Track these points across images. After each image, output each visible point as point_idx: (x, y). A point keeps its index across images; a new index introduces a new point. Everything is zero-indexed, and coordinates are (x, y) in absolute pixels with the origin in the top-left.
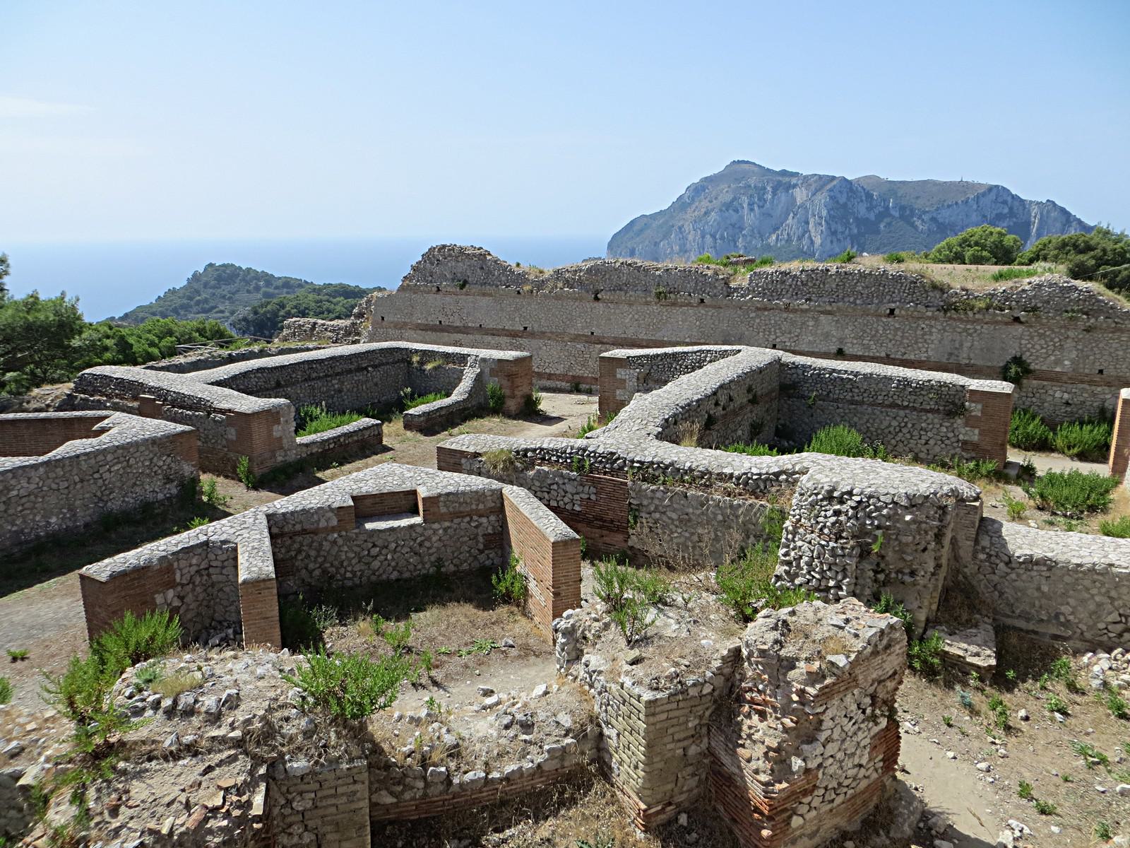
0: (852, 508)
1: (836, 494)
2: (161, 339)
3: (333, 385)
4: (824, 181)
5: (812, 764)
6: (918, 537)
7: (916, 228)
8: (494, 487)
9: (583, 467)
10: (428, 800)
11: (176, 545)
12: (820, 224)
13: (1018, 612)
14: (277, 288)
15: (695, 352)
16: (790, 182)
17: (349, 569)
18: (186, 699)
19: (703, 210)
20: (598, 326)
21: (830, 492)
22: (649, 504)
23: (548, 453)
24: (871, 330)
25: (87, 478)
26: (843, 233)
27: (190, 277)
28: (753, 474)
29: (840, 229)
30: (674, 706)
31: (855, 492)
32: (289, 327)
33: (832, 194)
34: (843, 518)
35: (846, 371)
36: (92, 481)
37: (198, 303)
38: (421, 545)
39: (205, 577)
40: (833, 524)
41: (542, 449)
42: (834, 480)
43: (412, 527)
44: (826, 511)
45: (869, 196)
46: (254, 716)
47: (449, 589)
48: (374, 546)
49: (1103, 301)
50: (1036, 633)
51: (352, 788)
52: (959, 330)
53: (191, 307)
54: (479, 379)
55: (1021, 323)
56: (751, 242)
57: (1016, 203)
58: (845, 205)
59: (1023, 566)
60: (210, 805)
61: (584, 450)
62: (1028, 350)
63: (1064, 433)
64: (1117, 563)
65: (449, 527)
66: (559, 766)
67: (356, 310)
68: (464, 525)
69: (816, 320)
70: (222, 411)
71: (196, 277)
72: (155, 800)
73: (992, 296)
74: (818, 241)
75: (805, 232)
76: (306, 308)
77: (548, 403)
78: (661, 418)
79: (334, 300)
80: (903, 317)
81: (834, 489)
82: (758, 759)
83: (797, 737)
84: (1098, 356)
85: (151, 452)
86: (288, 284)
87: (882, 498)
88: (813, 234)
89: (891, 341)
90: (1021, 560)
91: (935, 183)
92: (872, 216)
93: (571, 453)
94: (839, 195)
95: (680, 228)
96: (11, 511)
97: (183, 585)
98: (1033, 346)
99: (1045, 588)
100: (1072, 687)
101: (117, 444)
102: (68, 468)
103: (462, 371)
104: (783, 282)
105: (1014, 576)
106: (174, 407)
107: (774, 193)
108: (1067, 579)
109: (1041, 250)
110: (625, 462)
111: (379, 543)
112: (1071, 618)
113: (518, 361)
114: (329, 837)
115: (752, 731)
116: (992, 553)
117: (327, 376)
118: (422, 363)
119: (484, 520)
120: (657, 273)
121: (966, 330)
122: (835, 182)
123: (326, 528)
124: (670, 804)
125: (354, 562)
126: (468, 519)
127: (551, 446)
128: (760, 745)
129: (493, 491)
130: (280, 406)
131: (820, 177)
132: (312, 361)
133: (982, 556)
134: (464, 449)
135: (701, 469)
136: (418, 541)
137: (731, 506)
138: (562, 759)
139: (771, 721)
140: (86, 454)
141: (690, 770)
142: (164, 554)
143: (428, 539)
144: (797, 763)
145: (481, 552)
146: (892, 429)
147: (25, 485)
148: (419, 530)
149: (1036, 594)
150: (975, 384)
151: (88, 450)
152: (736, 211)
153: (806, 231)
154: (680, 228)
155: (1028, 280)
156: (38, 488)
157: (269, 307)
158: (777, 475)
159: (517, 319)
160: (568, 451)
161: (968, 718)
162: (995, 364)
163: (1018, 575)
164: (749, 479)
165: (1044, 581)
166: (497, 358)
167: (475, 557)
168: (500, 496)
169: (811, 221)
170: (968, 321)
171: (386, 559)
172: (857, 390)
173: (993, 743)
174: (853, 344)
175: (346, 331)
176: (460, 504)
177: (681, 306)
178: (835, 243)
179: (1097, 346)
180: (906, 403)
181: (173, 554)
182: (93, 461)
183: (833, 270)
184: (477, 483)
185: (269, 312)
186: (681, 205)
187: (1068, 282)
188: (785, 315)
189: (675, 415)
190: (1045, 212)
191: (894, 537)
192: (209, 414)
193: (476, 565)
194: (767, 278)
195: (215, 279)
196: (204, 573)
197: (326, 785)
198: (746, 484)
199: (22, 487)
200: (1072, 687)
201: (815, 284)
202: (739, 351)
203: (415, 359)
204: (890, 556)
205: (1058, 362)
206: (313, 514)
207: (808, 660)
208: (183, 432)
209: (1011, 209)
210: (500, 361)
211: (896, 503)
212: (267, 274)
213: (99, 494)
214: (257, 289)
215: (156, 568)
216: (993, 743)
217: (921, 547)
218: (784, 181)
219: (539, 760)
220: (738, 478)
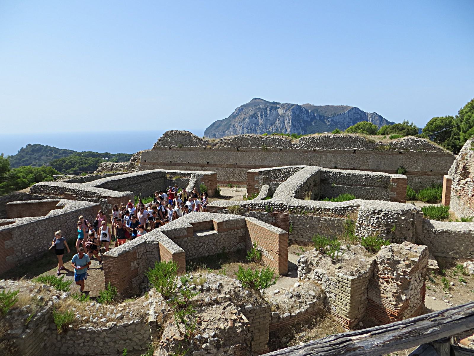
0: (383, 216)
1: (376, 211)
2: (27, 175)
3: (138, 187)
4: (289, 106)
5: (408, 298)
6: (407, 225)
7: (326, 123)
8: (242, 218)
9: (270, 209)
10: (272, 325)
11: (136, 243)
12: (289, 123)
13: (439, 250)
14: (60, 154)
15: (286, 169)
16: (276, 106)
17: (191, 252)
18: (206, 286)
19: (243, 118)
20: (239, 161)
21: (374, 211)
22: (297, 222)
23: (254, 205)
24: (347, 158)
25: (63, 225)
26: (298, 126)
27: (19, 150)
29: (297, 125)
30: (359, 281)
31: (383, 210)
32: (101, 166)
33: (293, 111)
34: (380, 220)
35: (346, 173)
36: (64, 226)
37: (23, 161)
38: (217, 241)
39: (145, 256)
40: (377, 222)
41: (252, 204)
42: (374, 207)
43: (214, 234)
44: (373, 218)
45: (307, 111)
46: (231, 290)
47: (227, 259)
48: (200, 242)
49: (430, 145)
50: (446, 257)
51: (265, 315)
52: (380, 157)
53: (20, 163)
54: (196, 183)
55: (402, 154)
56: (262, 130)
57: (362, 114)
58: (298, 115)
59: (440, 234)
60: (233, 319)
61: (270, 203)
62: (405, 164)
63: (421, 193)
64: (472, 230)
65: (227, 234)
66: (312, 310)
67: (132, 158)
68: (232, 233)
69: (326, 156)
70: (105, 197)
71: (22, 150)
72: (213, 318)
73: (391, 144)
74: (289, 130)
75: (284, 126)
76: (75, 163)
77: (224, 191)
78: (294, 190)
79: (88, 159)
80: (359, 153)
81: (375, 210)
82: (390, 297)
83: (402, 288)
84: (430, 165)
85: (85, 213)
86: (65, 152)
87: (393, 212)
88: (286, 127)
89: (355, 162)
90: (440, 231)
91: (332, 107)
92: (309, 120)
93: (264, 205)
94: (296, 111)
95: (234, 125)
96: (35, 239)
97: (139, 259)
98: (407, 162)
99: (448, 241)
100: (464, 274)
101: (73, 210)
102: (56, 221)
103: (188, 181)
104: (313, 141)
105: (437, 238)
106: (81, 197)
107: (270, 111)
108: (456, 237)
109: (386, 130)
110: (287, 207)
111: (202, 241)
112: (458, 251)
113: (212, 175)
114: (256, 334)
115: (386, 288)
116: (429, 230)
117: (136, 183)
118: (171, 178)
119: (239, 231)
120: (263, 139)
121: (382, 157)
122: (294, 107)
123: (183, 236)
124: (356, 319)
126: (233, 230)
127: (256, 202)
128: (390, 292)
129: (242, 219)
130: (129, 194)
131: (288, 104)
132: (130, 177)
133: (426, 231)
134: (218, 206)
135: (318, 207)
137: (331, 220)
138: (313, 307)
139: (391, 284)
140: (62, 215)
141: (362, 305)
142: (133, 246)
143: (220, 239)
144: (403, 297)
145: (238, 243)
146: (364, 194)
147: (41, 228)
148: (216, 235)
149: (445, 243)
150: (393, 176)
151: (63, 213)
152: (256, 118)
153: (284, 126)
154: (234, 125)
155: (403, 138)
156: (45, 229)
157: (58, 162)
158: (347, 207)
159: (204, 159)
160: (263, 204)
161: (434, 286)
162: (393, 169)
163: (439, 237)
164: (337, 210)
165: (447, 238)
166: (204, 174)
167: (236, 245)
168: (244, 221)
169: (286, 122)
170: (383, 154)
171: (204, 248)
172: (350, 180)
173: (446, 293)
174: (341, 164)
175: (128, 167)
176: (231, 225)
177: (272, 152)
178: (295, 130)
179: (429, 161)
180: (369, 184)
181: (136, 246)
182: (65, 218)
183: (332, 136)
184: (236, 217)
185: (58, 164)
186: (233, 116)
187: (418, 139)
188: (314, 154)
189: (298, 189)
190: (373, 117)
191: (398, 226)
192: (99, 199)
193: (236, 249)
194: (306, 140)
195: (31, 151)
196: (145, 254)
197: (257, 314)
198: (336, 211)
199: (40, 229)
200: (464, 274)
201: (325, 142)
202: (304, 167)
203: (168, 176)
204: (397, 233)
205: (416, 168)
206: (178, 231)
207: (404, 260)
208: (96, 205)
209: (361, 116)
211: (398, 213)
212: (55, 148)
213: (67, 231)
214: (51, 154)
215: (132, 252)
216: (446, 293)
217: (408, 229)
218: (274, 106)
219: (306, 308)
220: (332, 210)
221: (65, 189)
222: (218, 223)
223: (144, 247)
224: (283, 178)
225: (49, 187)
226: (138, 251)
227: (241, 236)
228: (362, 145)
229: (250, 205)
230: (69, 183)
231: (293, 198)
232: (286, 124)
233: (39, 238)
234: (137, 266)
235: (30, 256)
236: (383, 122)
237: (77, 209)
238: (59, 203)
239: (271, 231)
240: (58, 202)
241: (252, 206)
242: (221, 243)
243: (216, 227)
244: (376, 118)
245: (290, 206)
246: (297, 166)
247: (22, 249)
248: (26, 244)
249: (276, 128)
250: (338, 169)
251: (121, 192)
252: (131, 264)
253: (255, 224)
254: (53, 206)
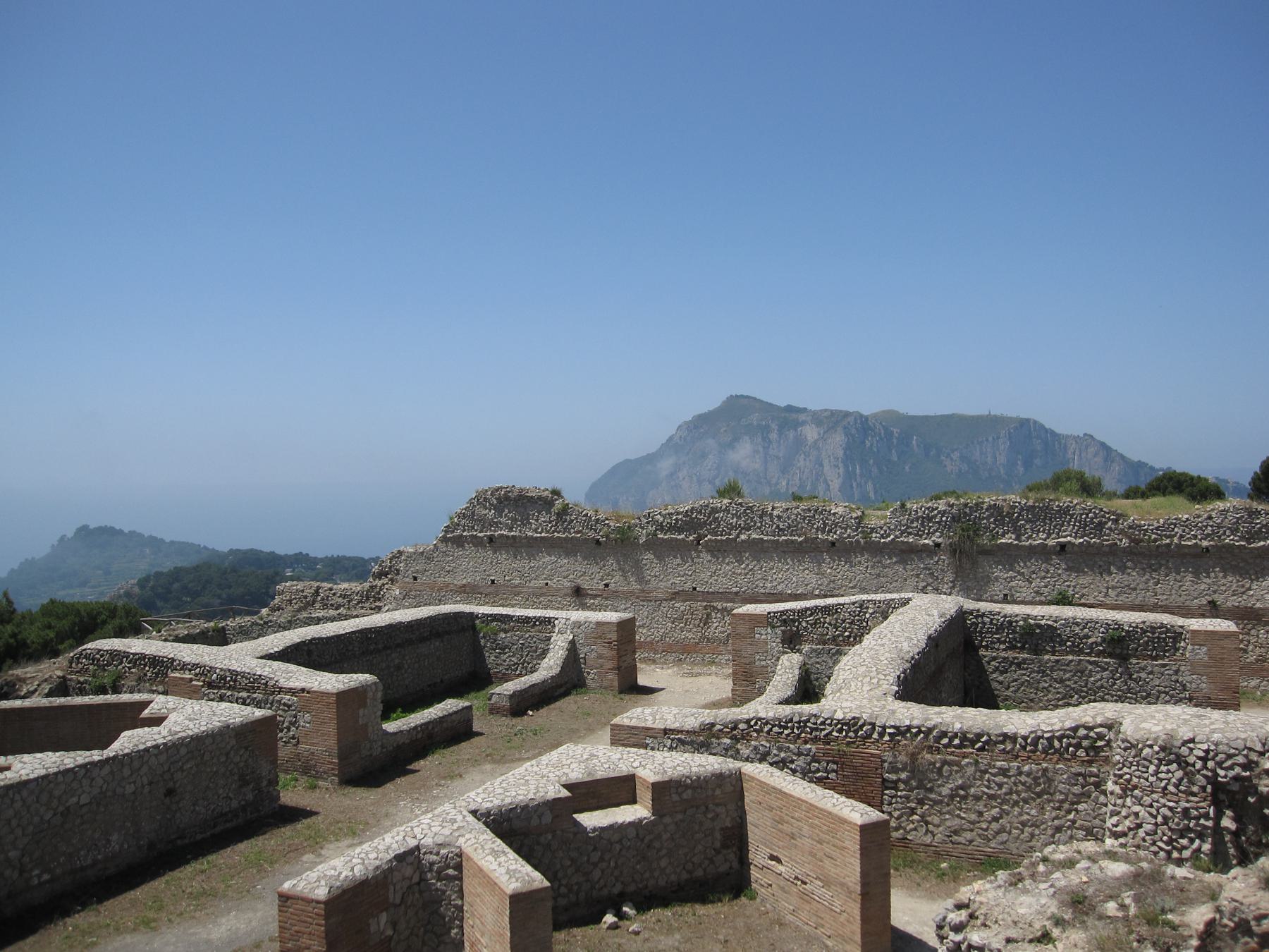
0: (1199, 758)
4: (833, 420)
15: (854, 604)
17: (564, 882)
28: (1044, 732)
39: (417, 895)
54: (573, 648)
70: (292, 691)
93: (799, 722)
97: (396, 906)
110: (873, 728)
125: (570, 871)
136: (646, 841)
145: (718, 852)
150: (1195, 624)
166: (594, 620)
169: (826, 463)
210: (598, 624)
221: (170, 664)
222: (653, 784)
223: (412, 864)
224: (847, 634)
225: (127, 654)
226: (395, 881)
227: (727, 828)
228: (1084, 528)
229: (752, 723)
230: (186, 645)
231: (891, 699)
232: (827, 468)
233: (79, 821)
234: (389, 932)
235: (48, 882)
236: (1112, 462)
237: (205, 728)
238: (149, 708)
239: (830, 813)
240: (146, 704)
241: (756, 725)
242: (664, 852)
243: (645, 796)
244: (1092, 450)
245: (884, 728)
246: (889, 596)
247: (23, 856)
249: (797, 481)
250: (1015, 602)
251: (341, 677)
252: (369, 925)
253: (773, 788)
254: (132, 716)
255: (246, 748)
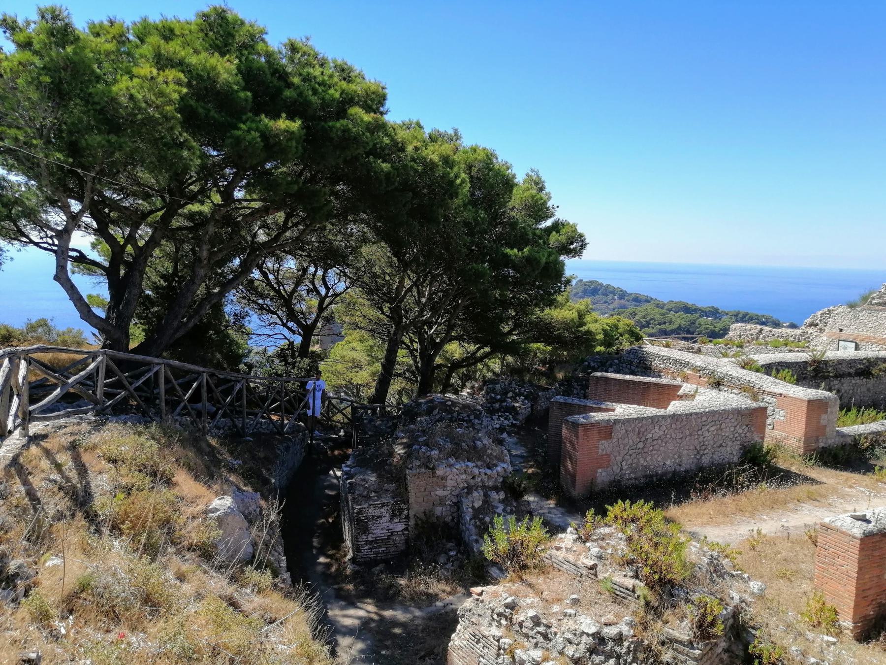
96: (646, 450)
101: (715, 409)
140: (696, 414)
147: (657, 430)
151: (698, 411)
213: (698, 448)
233: (651, 448)
248: (631, 455)
255: (747, 426)
